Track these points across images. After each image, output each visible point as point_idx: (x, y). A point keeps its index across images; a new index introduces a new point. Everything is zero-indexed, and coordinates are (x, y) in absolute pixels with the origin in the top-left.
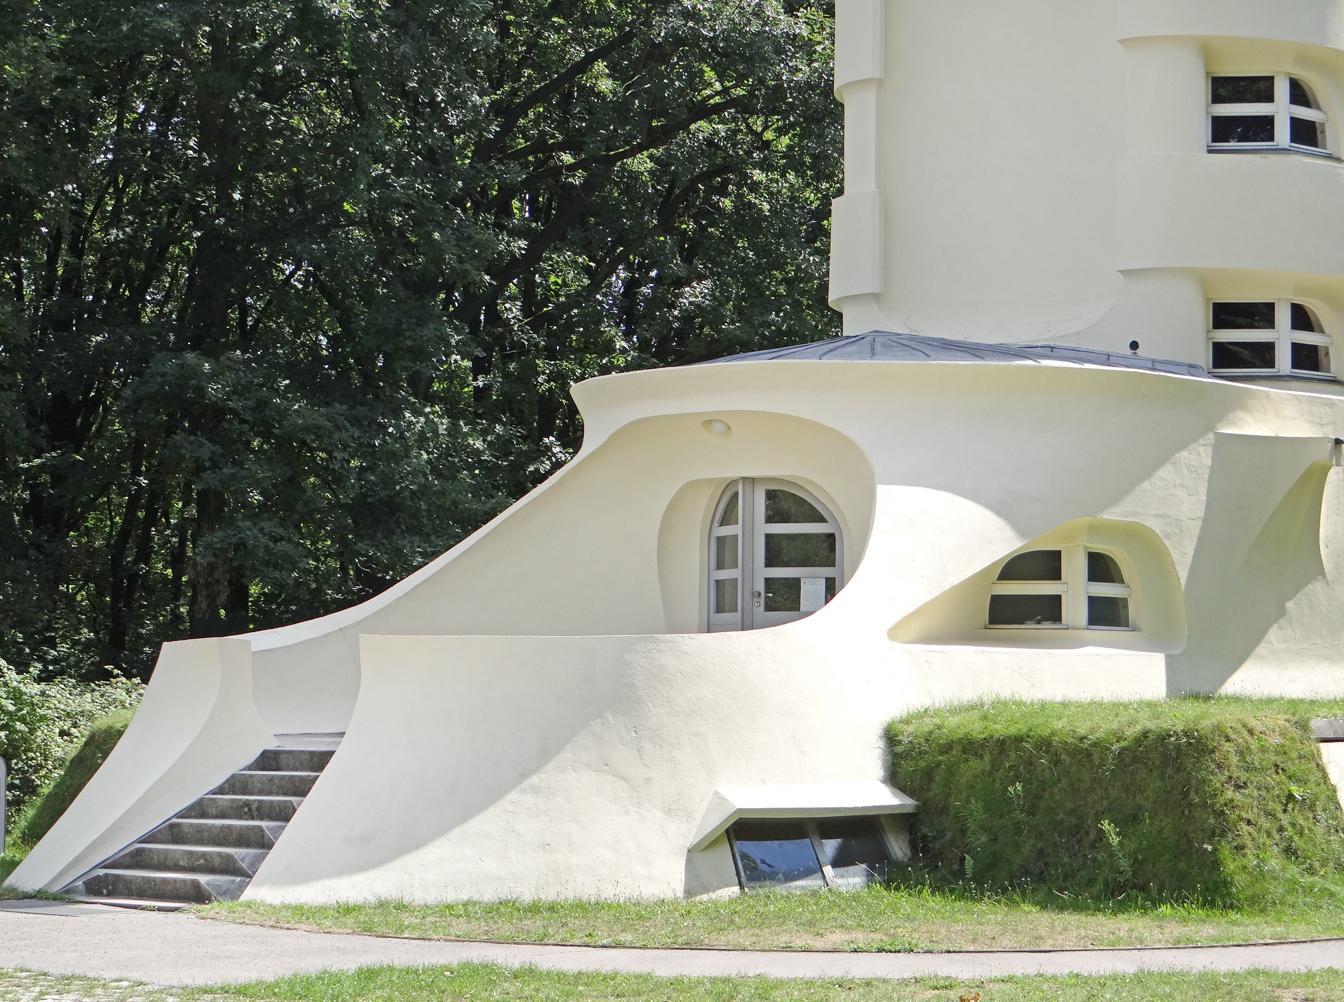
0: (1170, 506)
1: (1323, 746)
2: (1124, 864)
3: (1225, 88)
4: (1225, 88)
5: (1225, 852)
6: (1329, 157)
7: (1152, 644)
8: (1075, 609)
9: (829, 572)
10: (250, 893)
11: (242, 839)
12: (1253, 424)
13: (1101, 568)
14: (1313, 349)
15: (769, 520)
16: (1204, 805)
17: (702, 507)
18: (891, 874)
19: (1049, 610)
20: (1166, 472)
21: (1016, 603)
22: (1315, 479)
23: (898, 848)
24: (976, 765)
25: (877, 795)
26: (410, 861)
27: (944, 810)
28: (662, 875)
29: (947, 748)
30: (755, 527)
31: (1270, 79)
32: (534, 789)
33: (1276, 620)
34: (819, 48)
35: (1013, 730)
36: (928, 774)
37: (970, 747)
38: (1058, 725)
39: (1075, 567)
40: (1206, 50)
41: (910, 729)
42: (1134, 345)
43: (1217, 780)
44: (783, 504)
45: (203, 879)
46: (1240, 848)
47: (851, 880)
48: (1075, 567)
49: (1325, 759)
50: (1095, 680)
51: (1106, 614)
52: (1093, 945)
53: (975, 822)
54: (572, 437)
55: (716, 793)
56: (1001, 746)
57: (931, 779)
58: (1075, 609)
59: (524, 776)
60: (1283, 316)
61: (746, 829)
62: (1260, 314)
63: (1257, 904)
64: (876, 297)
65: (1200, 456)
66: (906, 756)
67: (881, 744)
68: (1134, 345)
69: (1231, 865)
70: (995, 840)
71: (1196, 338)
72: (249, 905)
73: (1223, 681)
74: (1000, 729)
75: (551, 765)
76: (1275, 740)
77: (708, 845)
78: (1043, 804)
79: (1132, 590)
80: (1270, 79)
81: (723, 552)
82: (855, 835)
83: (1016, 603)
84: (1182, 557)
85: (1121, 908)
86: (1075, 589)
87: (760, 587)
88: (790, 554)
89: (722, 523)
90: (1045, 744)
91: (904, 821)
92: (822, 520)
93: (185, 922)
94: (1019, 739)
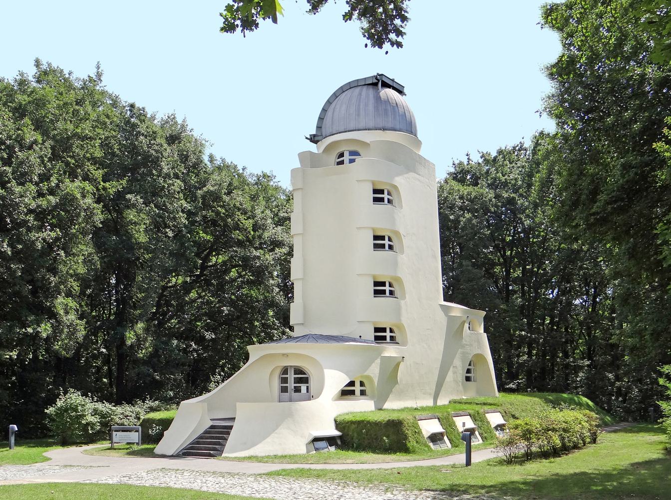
0: (374, 371)
1: (419, 421)
2: (388, 445)
3: (376, 284)
4: (376, 284)
5: (407, 442)
6: (396, 297)
7: (372, 398)
8: (358, 392)
9: (307, 385)
10: (224, 455)
11: (219, 444)
12: (386, 354)
13: (362, 384)
14: (469, 377)
15: (295, 374)
16: (402, 434)
17: (278, 371)
18: (338, 447)
19: (352, 393)
20: (373, 364)
21: (347, 393)
22: (398, 365)
23: (339, 442)
24: (353, 426)
25: (337, 433)
26: (255, 448)
27: (348, 435)
28: (302, 450)
29: (348, 422)
30: (291, 376)
31: (385, 282)
32: (276, 433)
33: (390, 393)
34: (262, 258)
35: (361, 419)
36: (344, 428)
37: (352, 422)
38: (370, 418)
39: (357, 384)
40: (374, 277)
41: (338, 419)
42: (360, 337)
43: (404, 429)
44: (298, 371)
45: (212, 452)
46: (410, 442)
47: (332, 449)
48: (357, 384)
49: (419, 424)
50: (361, 408)
51: (363, 393)
52: (384, 462)
53: (352, 437)
54: (247, 358)
55: (310, 433)
56: (359, 423)
57: (344, 429)
58: (358, 392)
59: (274, 431)
60: (388, 330)
61: (316, 439)
62: (384, 330)
63: (414, 452)
64: (303, 324)
65: (378, 361)
66: (339, 425)
67: (334, 422)
68: (360, 337)
69: (409, 445)
70: (359, 440)
71: (371, 335)
72: (223, 457)
73: (383, 406)
74: (358, 419)
75: (280, 428)
76: (412, 421)
77: (309, 443)
78: (369, 433)
79: (367, 388)
80: (385, 282)
81: (284, 380)
82: (331, 441)
83: (347, 393)
84: (376, 380)
85: (390, 453)
86: (357, 388)
87: (293, 388)
88: (297, 382)
89: (283, 374)
90: (368, 422)
91: (340, 437)
92: (305, 374)
93: (211, 461)
94: (363, 421)
